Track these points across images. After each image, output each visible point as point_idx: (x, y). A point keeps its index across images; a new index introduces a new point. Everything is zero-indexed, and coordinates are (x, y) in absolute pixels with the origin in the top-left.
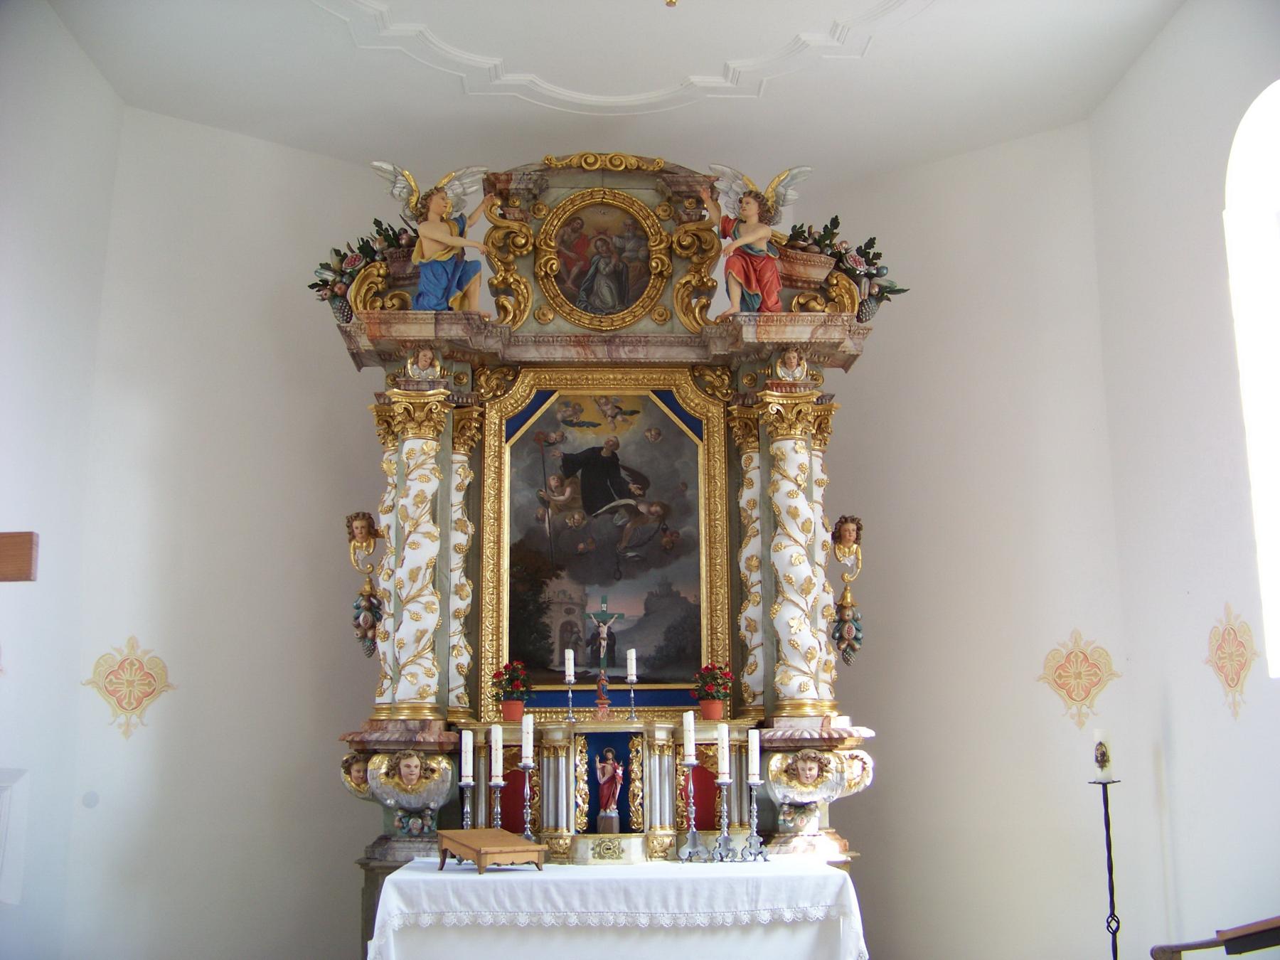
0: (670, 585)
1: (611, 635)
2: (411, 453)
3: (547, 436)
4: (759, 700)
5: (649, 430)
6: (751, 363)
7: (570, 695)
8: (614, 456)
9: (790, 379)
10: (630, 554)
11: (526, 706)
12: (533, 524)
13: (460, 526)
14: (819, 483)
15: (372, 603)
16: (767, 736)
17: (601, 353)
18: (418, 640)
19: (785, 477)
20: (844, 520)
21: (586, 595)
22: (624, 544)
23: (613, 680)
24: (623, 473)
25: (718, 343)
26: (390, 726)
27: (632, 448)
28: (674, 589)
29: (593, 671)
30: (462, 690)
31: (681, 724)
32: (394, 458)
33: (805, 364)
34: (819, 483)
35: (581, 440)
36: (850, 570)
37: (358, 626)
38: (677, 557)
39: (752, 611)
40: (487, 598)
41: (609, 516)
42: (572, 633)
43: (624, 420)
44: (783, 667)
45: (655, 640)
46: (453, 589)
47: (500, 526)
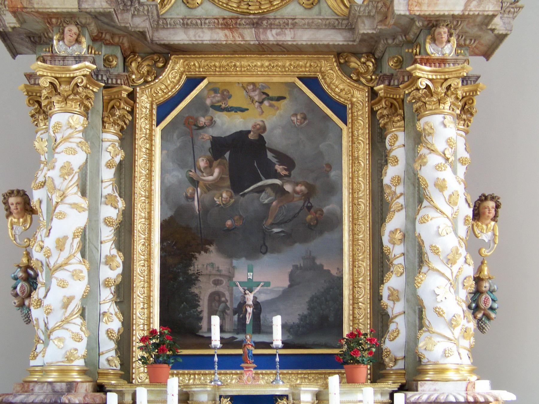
0: (314, 259)
1: (257, 305)
2: (58, 125)
3: (196, 120)
4: (400, 365)
5: (295, 115)
6: (397, 46)
7: (216, 359)
8: (261, 138)
9: (437, 56)
10: (276, 230)
11: (172, 368)
12: (183, 202)
13: (110, 201)
14: (462, 161)
15: (29, 275)
16: (412, 399)
17: (249, 36)
18: (65, 306)
19: (432, 151)
20: (484, 198)
21: (234, 268)
22: (270, 221)
23: (258, 345)
24: (270, 155)
25: (366, 22)
26: (37, 388)
27: (278, 131)
28: (318, 262)
29: (240, 337)
30: (113, 353)
31: (326, 386)
32: (45, 137)
33: (454, 39)
34: (462, 161)
35: (229, 124)
36: (487, 246)
37: (16, 295)
38: (321, 233)
39: (395, 282)
40: (139, 268)
41: (255, 195)
42: (220, 302)
43: (271, 106)
44: (427, 334)
45: (299, 308)
46: (103, 260)
47: (150, 204)
